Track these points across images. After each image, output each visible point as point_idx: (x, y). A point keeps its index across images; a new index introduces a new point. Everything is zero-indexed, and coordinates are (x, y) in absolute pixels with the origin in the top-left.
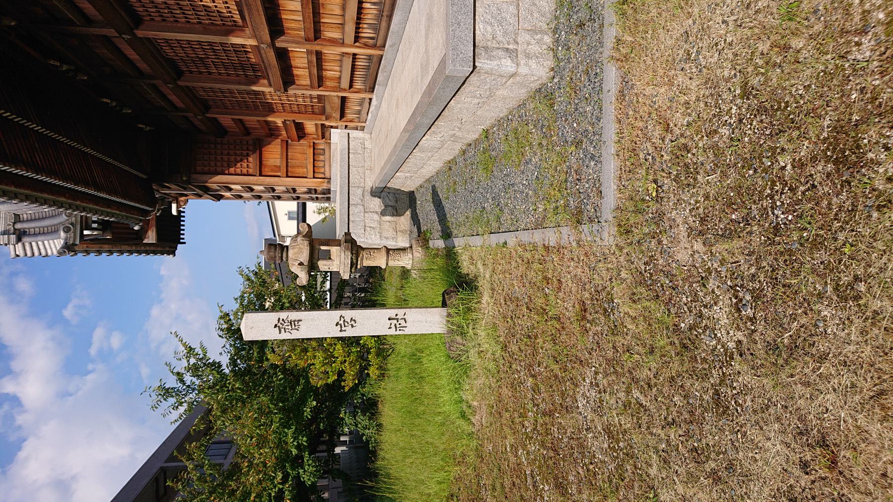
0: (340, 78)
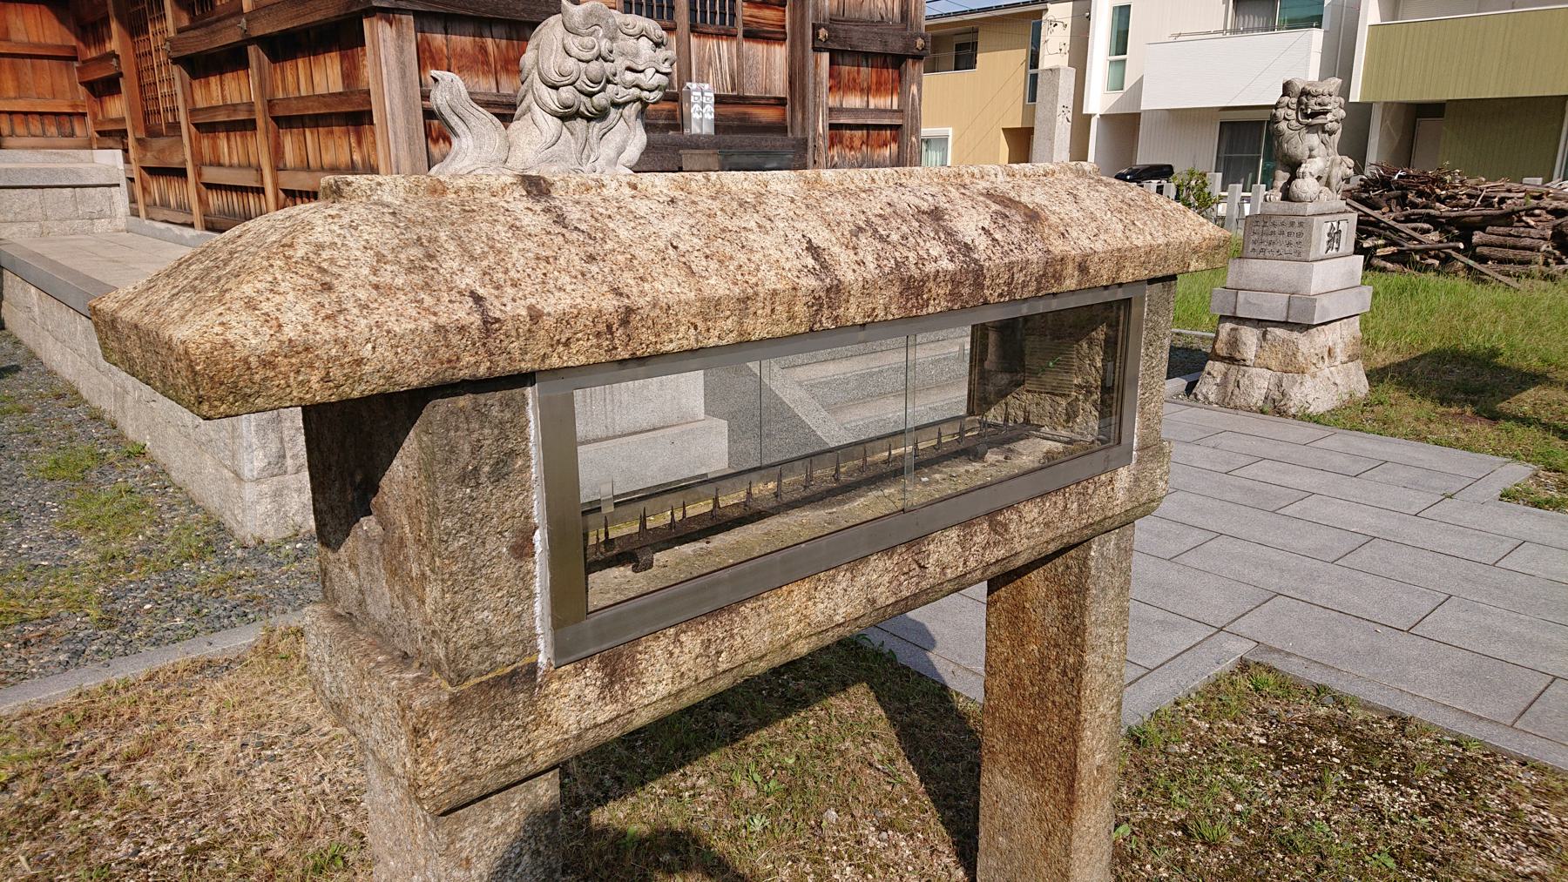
0: (220, 165)
